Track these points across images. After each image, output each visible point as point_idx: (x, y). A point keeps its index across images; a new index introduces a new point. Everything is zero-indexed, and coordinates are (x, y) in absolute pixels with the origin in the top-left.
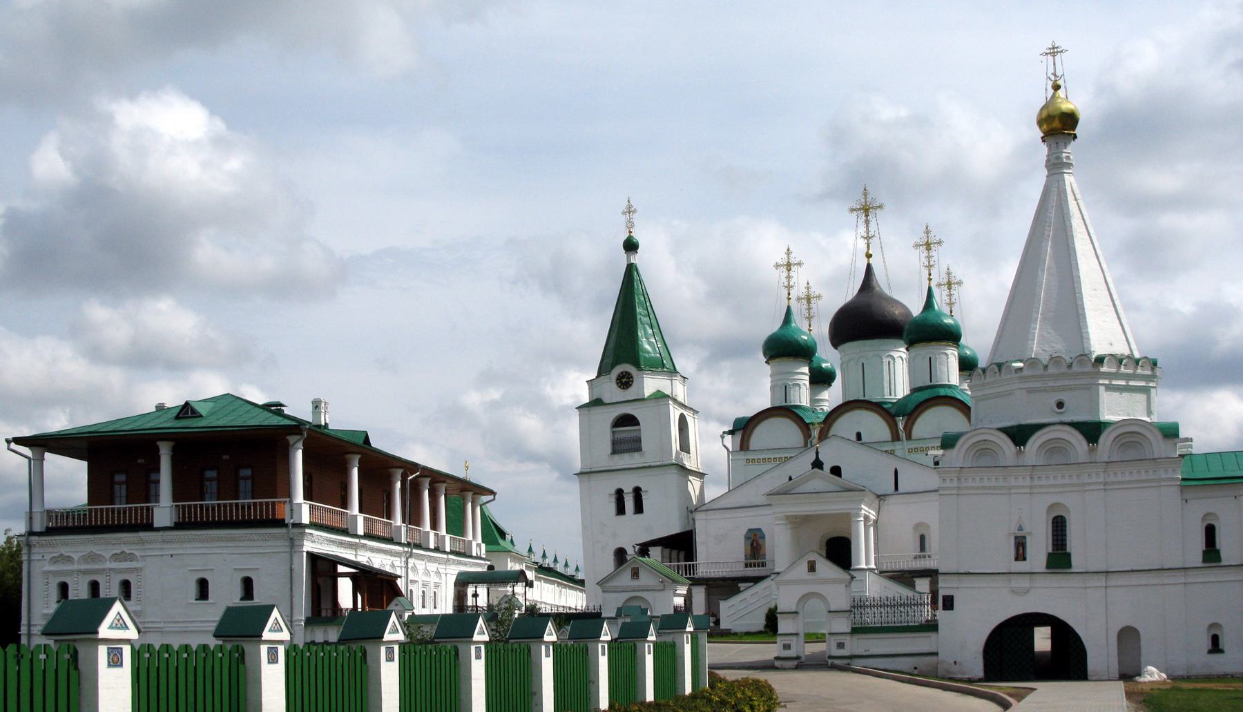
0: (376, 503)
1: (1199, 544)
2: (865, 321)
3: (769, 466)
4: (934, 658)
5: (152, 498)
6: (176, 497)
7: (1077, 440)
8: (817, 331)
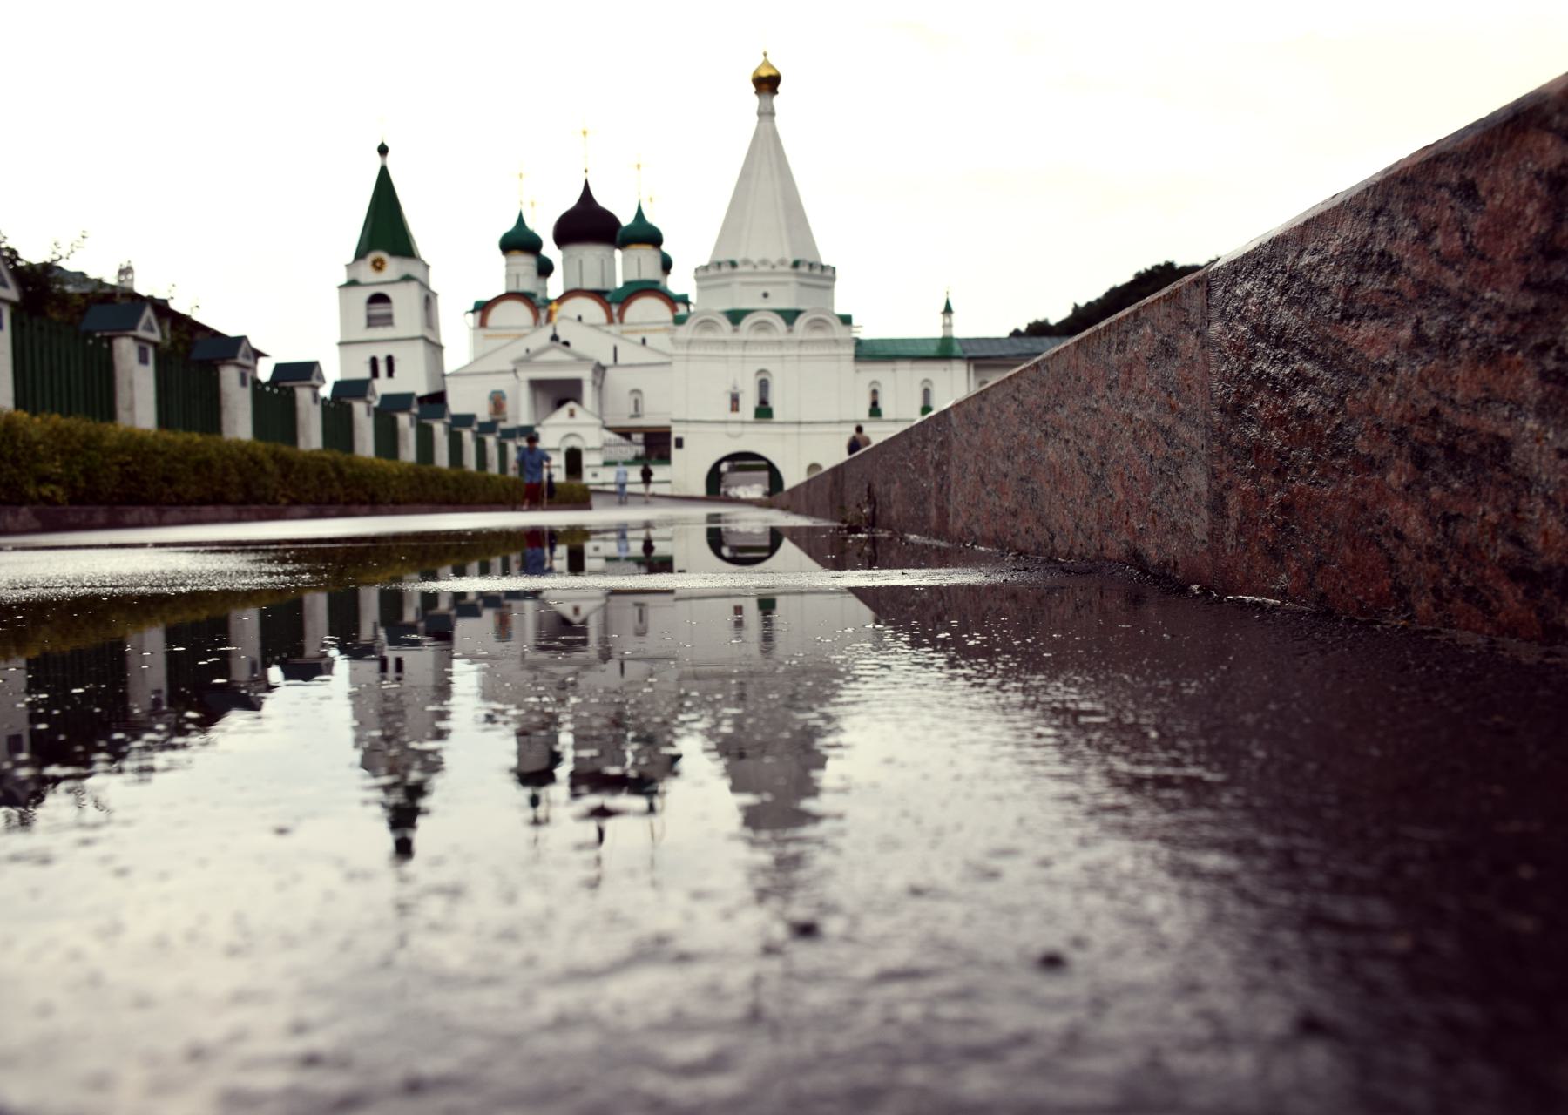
1: (867, 405)
2: (587, 224)
3: (505, 341)
7: (779, 323)
8: (543, 228)
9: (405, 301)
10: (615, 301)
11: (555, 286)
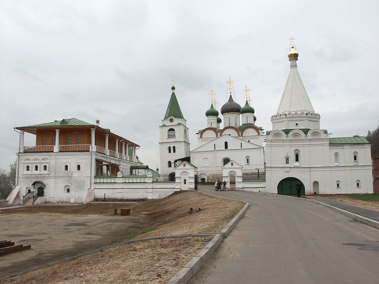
0: (112, 147)
2: (231, 108)
4: (265, 188)
5: (53, 144)
6: (60, 143)
8: (219, 109)
9: (179, 132)
10: (241, 130)
11: (222, 126)
